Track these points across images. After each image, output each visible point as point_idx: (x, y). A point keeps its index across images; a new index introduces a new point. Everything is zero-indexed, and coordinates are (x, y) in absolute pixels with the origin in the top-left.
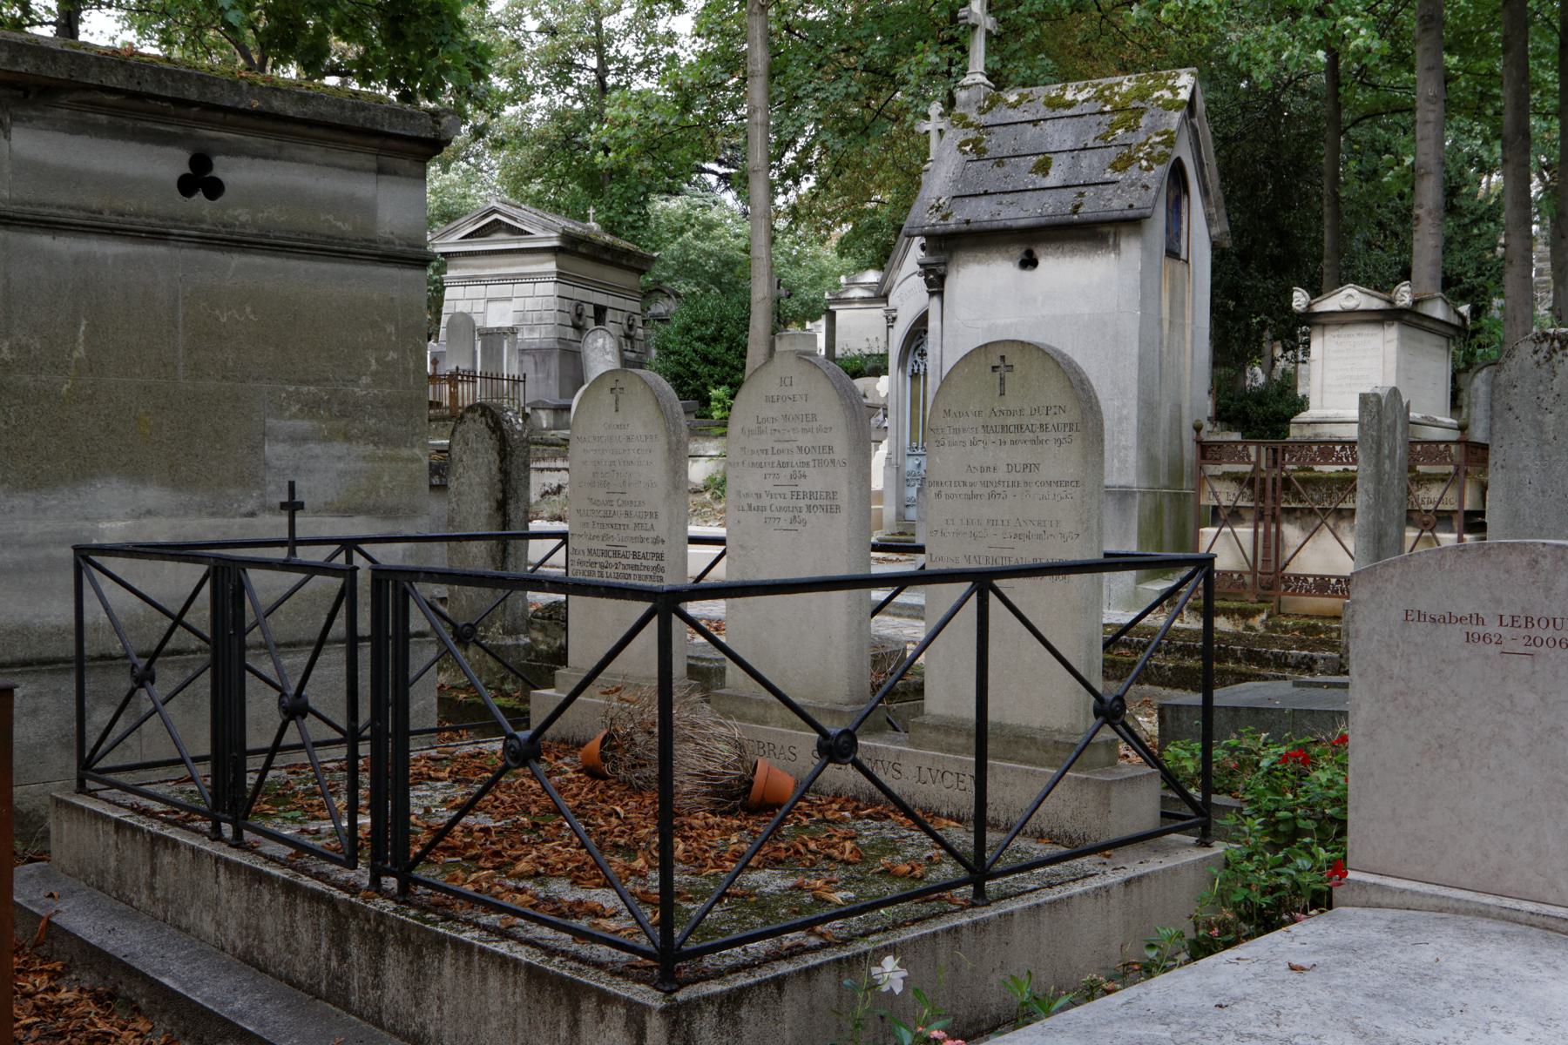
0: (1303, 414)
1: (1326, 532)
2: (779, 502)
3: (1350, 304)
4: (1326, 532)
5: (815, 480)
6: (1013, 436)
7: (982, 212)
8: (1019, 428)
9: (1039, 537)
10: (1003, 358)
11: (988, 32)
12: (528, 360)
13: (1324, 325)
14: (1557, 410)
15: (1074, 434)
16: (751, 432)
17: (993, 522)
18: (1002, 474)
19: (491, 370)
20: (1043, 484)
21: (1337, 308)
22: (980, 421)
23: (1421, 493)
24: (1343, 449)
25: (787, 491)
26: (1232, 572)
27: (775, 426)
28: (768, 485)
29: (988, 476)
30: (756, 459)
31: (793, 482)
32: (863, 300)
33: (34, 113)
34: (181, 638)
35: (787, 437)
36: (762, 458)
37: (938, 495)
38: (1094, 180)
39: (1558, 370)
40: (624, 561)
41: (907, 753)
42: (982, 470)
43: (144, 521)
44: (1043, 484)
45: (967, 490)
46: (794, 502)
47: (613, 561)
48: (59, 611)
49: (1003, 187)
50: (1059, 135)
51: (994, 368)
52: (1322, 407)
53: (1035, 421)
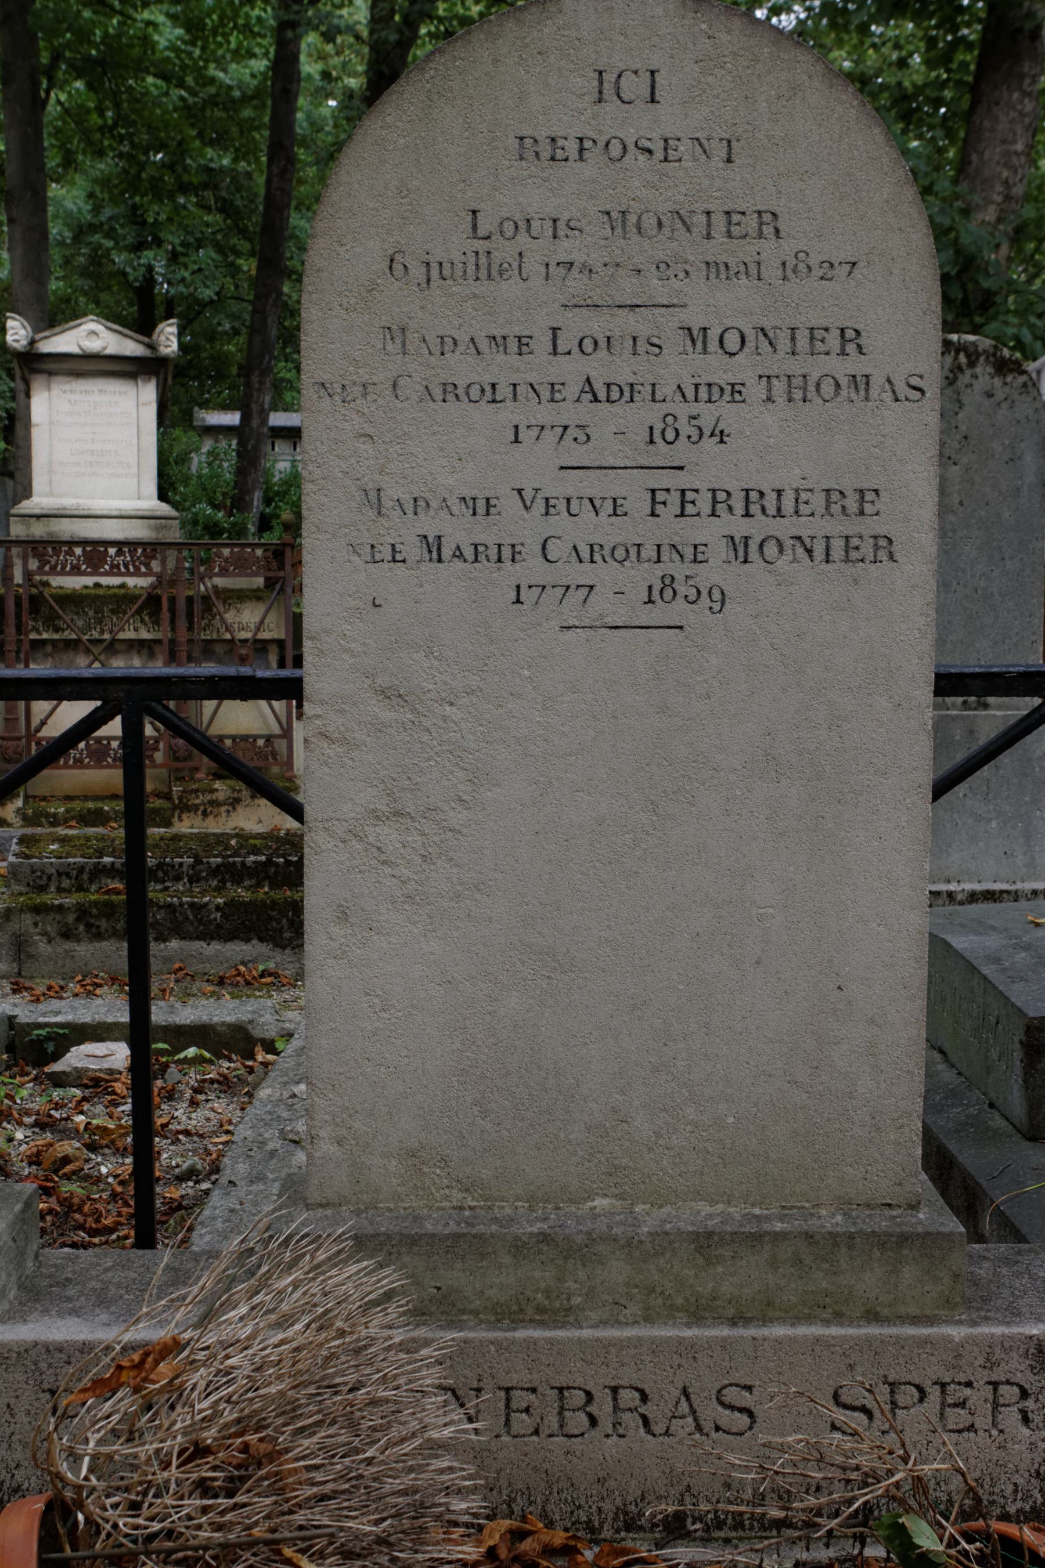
0: (25, 503)
2: (590, 527)
3: (94, 345)
5: (771, 446)
13: (51, 374)
14: (965, 460)
16: (435, 272)
21: (74, 349)
23: (230, 616)
24: (120, 553)
25: (633, 489)
26: (255, 738)
27: (569, 248)
28: (538, 465)
30: (463, 369)
31: (662, 454)
35: (628, 289)
36: (502, 368)
39: (965, 399)
46: (668, 527)
52: (51, 494)
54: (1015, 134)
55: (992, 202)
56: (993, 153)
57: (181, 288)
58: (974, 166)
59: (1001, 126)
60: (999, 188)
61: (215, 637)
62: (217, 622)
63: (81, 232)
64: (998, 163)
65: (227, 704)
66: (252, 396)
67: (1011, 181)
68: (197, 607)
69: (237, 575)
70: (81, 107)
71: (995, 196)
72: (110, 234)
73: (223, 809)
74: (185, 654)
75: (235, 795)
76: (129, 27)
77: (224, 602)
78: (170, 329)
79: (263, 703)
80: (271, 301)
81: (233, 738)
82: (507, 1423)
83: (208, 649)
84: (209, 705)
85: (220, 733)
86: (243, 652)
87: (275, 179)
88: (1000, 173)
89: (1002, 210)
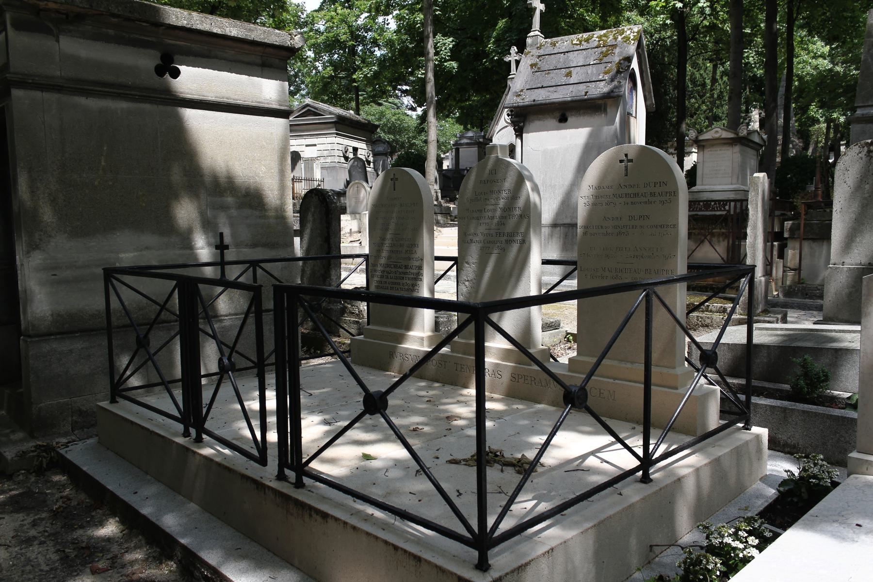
1: (707, 243)
4: (707, 243)
7: (541, 96)
11: (541, 11)
12: (325, 172)
19: (309, 177)
21: (710, 137)
32: (467, 144)
33: (72, 28)
34: (164, 315)
38: (594, 79)
40: (400, 270)
43: (144, 253)
47: (393, 270)
48: (99, 303)
49: (550, 84)
50: (577, 59)
52: (702, 185)
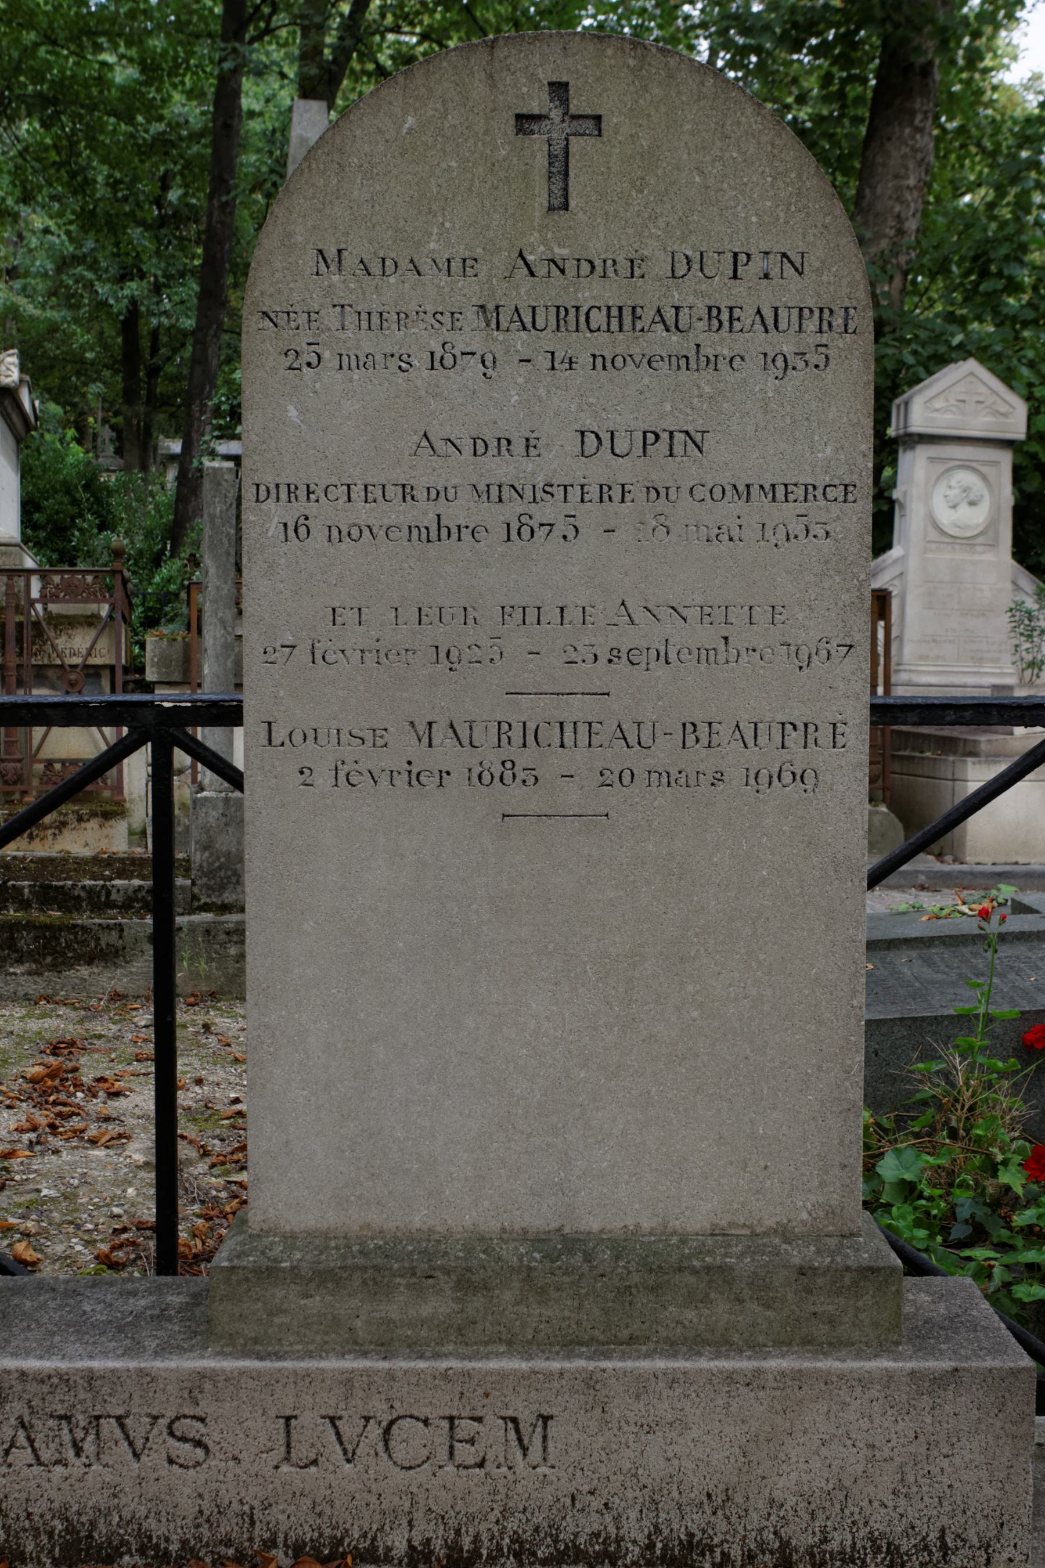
6: (603, 343)
8: (624, 317)
9: (705, 655)
10: (559, 89)
15: (838, 342)
17: (528, 615)
18: (559, 461)
20: (718, 493)
22: (468, 291)
23: (61, 642)
29: (501, 469)
37: (297, 529)
41: (232, 1379)
42: (479, 446)
44: (718, 493)
45: (424, 514)
51: (525, 122)
53: (692, 294)
54: (907, 169)
55: (885, 236)
56: (885, 188)
57: (165, 321)
58: (867, 199)
59: (892, 162)
60: (891, 222)
61: (46, 662)
62: (48, 647)
63: (64, 263)
64: (890, 198)
65: (55, 730)
66: (192, 425)
67: (903, 215)
68: (28, 633)
69: (67, 602)
70: (41, 144)
71: (887, 230)
72: (94, 267)
73: (50, 832)
74: (14, 679)
75: (62, 818)
76: (85, 67)
77: (56, 627)
78: (10, 359)
79: (94, 730)
80: (212, 332)
81: (63, 762)
82: (451, 1454)
83: (41, 676)
84: (38, 732)
85: (50, 757)
86: (73, 677)
87: (216, 213)
88: (892, 208)
89: (894, 243)
